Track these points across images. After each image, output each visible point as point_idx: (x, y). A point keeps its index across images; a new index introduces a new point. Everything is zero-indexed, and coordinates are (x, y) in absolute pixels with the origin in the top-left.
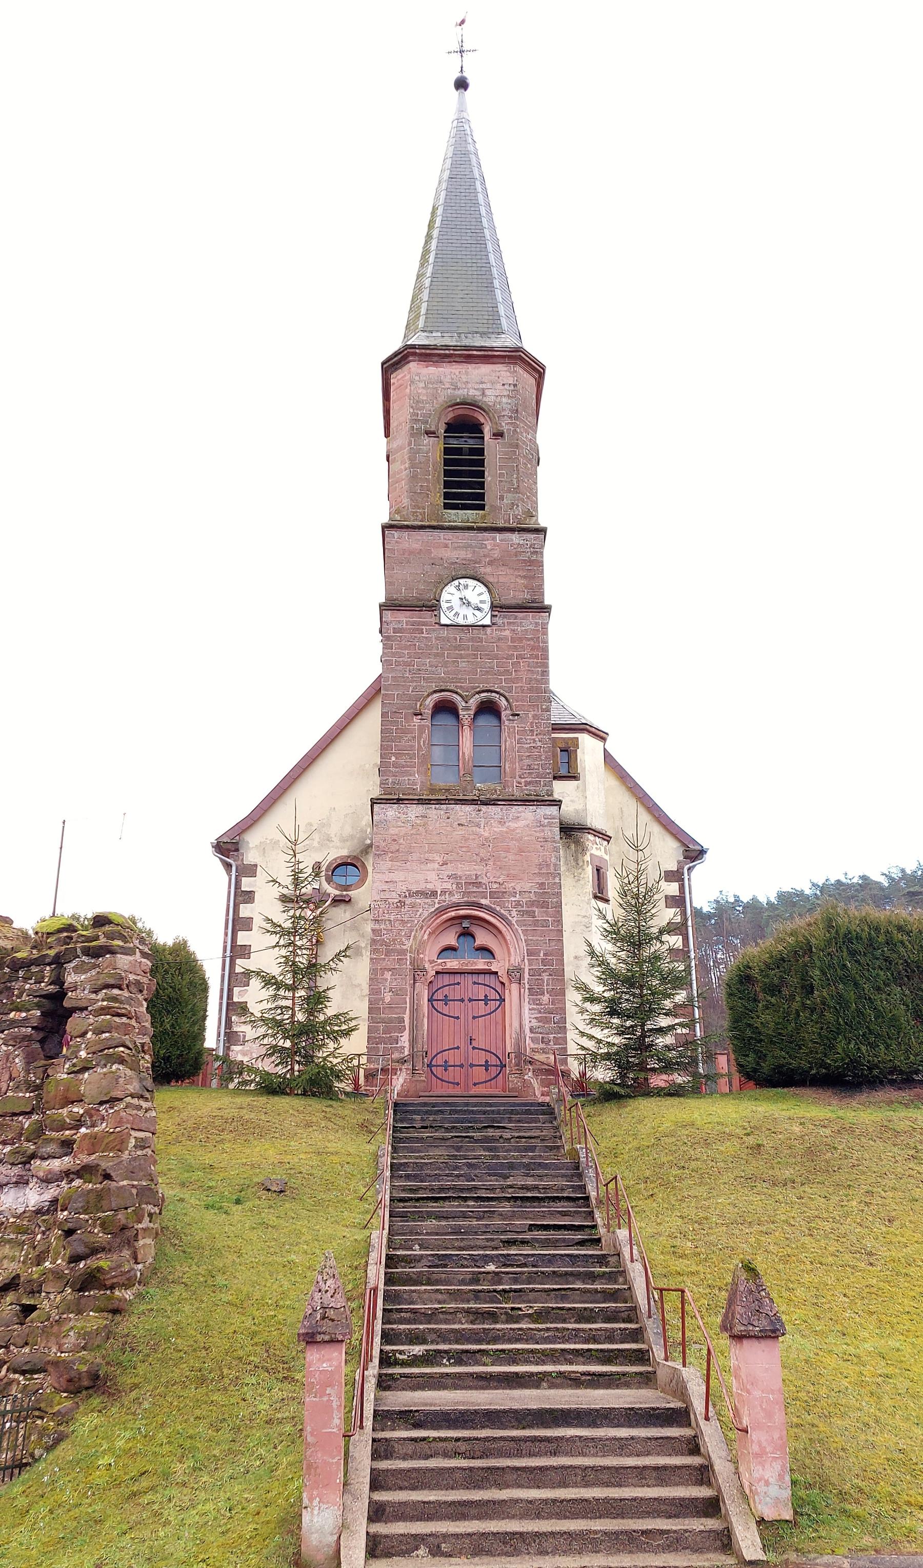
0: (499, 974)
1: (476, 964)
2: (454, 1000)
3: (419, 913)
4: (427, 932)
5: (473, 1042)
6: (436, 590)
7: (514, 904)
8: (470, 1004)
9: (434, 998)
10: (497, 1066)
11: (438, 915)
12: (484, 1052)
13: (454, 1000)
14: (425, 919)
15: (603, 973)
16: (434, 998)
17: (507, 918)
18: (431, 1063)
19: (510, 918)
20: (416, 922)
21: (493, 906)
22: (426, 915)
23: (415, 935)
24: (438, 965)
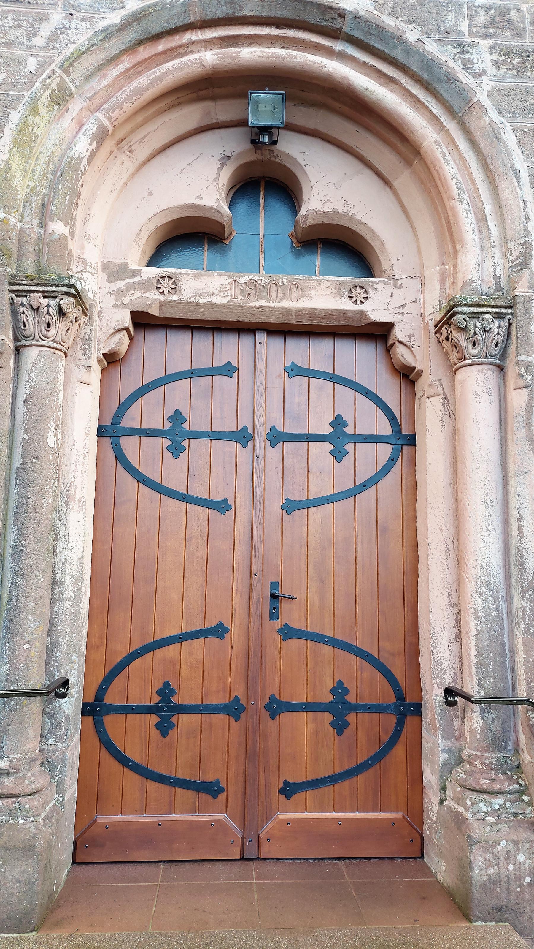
0: (399, 333)
1: (302, 290)
2: (210, 436)
3: (46, 30)
4: (91, 126)
5: (284, 606)
6: (508, 314)
7: (481, 18)
8: (245, 421)
9: (127, 422)
10: (379, 709)
11: (144, 53)
12: (327, 650)
13: (210, 436)
14: (79, 56)
15: (496, 881)
16: (127, 422)
17: (451, 80)
18: (400, 724)
19: (464, 77)
20: (32, 64)
21: (390, 22)
22: (82, 39)
23: (24, 125)
24: (146, 285)
